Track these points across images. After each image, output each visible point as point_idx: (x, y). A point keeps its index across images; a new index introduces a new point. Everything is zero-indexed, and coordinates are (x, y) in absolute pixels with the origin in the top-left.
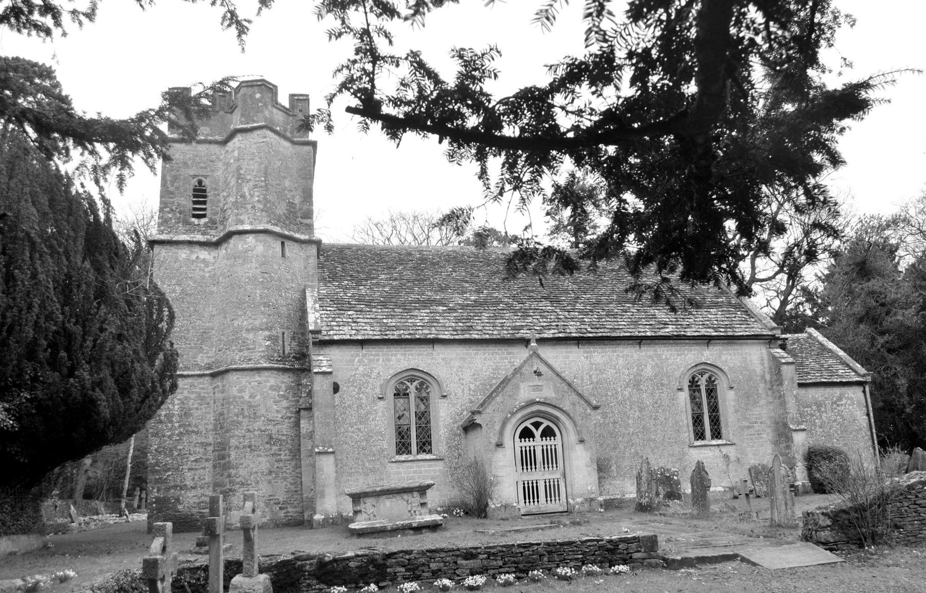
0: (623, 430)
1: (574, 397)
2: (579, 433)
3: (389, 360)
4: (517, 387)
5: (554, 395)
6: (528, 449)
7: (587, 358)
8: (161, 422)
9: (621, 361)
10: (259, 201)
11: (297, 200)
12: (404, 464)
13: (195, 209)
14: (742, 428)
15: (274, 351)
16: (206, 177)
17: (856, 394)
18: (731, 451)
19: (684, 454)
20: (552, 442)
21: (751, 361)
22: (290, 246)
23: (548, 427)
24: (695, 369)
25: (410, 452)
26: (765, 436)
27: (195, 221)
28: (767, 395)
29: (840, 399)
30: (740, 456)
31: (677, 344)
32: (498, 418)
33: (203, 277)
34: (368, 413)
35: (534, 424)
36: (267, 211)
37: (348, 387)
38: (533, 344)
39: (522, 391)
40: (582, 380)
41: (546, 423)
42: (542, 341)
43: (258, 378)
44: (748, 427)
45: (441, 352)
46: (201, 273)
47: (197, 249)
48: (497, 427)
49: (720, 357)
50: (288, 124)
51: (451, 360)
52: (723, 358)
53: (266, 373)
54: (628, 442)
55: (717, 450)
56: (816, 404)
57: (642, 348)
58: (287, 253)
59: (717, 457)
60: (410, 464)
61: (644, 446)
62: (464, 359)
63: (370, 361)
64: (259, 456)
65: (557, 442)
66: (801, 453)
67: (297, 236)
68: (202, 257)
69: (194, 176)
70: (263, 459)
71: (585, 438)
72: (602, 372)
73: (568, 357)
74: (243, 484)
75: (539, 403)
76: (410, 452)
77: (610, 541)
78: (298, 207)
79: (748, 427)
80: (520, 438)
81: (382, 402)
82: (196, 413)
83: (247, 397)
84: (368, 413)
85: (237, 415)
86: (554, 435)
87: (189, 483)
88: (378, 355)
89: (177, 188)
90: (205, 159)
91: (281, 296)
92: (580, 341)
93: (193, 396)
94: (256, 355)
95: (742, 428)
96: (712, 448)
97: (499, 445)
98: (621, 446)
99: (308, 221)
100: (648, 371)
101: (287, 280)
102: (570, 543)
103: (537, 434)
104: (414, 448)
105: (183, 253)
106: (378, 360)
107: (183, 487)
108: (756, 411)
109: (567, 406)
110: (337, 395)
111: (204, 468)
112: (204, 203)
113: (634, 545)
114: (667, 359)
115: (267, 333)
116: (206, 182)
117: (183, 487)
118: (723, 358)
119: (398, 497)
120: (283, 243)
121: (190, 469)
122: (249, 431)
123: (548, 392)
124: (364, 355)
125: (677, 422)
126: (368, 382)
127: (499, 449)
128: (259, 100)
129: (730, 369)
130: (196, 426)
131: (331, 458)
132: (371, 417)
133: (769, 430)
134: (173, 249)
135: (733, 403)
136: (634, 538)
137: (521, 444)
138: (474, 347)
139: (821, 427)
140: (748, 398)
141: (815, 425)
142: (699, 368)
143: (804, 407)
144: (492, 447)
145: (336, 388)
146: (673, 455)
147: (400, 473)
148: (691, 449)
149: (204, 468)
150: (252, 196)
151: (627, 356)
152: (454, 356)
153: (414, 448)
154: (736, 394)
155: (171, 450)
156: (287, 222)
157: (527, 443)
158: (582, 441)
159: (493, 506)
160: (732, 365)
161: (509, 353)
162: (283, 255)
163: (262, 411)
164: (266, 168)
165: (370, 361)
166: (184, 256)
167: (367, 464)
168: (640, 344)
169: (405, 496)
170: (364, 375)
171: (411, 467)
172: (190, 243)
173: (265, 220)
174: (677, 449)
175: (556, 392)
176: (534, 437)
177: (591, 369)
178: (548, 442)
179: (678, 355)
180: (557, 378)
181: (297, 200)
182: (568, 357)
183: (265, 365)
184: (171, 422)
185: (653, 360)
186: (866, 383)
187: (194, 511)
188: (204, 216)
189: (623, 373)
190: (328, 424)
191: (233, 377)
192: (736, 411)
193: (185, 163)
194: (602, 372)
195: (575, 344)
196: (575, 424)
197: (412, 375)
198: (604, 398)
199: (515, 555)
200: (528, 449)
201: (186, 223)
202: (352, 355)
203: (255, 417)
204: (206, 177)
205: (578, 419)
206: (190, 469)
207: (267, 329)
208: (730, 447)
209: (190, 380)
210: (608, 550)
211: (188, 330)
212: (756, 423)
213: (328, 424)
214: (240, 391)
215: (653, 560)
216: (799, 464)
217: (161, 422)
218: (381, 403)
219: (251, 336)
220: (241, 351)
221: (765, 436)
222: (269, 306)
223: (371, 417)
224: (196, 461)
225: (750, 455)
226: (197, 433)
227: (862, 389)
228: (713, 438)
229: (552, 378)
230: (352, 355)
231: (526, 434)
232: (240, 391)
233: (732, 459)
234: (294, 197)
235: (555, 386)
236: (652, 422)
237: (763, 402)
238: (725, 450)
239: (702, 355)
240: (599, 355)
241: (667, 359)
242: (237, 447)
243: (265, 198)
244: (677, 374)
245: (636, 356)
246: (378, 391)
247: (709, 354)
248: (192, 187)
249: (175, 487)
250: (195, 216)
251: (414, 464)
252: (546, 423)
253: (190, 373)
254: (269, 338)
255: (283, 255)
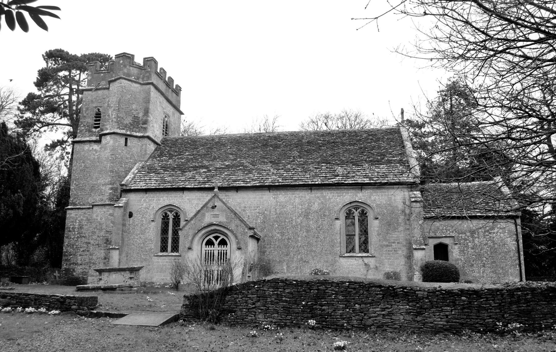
0: (293, 244)
1: (238, 222)
2: (238, 243)
3: (159, 200)
4: (204, 215)
5: (225, 220)
6: (225, 252)
7: (274, 198)
8: (70, 231)
9: (297, 200)
10: (115, 118)
11: (141, 115)
12: (162, 258)
13: (95, 124)
14: (382, 246)
15: (115, 195)
16: (101, 107)
17: (510, 226)
18: (372, 262)
19: (336, 261)
20: (225, 248)
21: (395, 200)
22: (130, 140)
23: (223, 239)
24: (349, 206)
25: (167, 251)
26: (400, 252)
27: (94, 130)
28: (406, 224)
29: (493, 228)
30: (378, 265)
31: (338, 189)
32: (191, 233)
33: (94, 158)
34: (146, 229)
35: (215, 237)
36: (118, 122)
37: (137, 214)
38: (216, 190)
39: (206, 218)
40: (270, 212)
41: (222, 237)
42: (220, 189)
43: (104, 210)
44: (387, 246)
45: (187, 195)
46: (94, 156)
47: (93, 144)
48: (190, 238)
49: (370, 197)
50: (141, 74)
51: (193, 199)
52: (373, 198)
53: (108, 207)
54: (296, 252)
55: (360, 260)
56: (470, 231)
57: (313, 192)
58: (129, 143)
59: (360, 265)
60: (164, 257)
61: (307, 254)
62: (200, 199)
63: (150, 200)
64: (101, 250)
65: (227, 248)
66: (419, 265)
67: (135, 134)
68: (94, 148)
69: (96, 107)
70: (103, 251)
71: (242, 247)
72: (284, 207)
73: (262, 198)
74: (94, 263)
75: (217, 225)
76: (167, 251)
77: (62, 297)
78: (140, 119)
79: (387, 246)
80: (206, 245)
81: (153, 223)
82: (85, 227)
83: (99, 219)
84: (146, 229)
85: (94, 228)
86: (227, 245)
87: (79, 262)
88: (154, 197)
89: (87, 114)
90: (101, 98)
91: (122, 166)
92: (270, 188)
93: (84, 219)
94: (105, 198)
95: (382, 246)
96: (357, 259)
97: (190, 248)
98: (292, 254)
99: (145, 126)
100: (316, 207)
101: (127, 158)
102: (45, 296)
103: (216, 243)
104: (169, 248)
105: (86, 147)
106: (154, 200)
107: (77, 264)
108: (395, 235)
109: (232, 227)
110: (131, 218)
111: (86, 255)
112: (99, 120)
113: (73, 301)
114: (330, 199)
115: (110, 186)
116: (101, 110)
117: (77, 264)
118: (373, 198)
119: (119, 273)
120: (126, 139)
121: (80, 255)
122: (98, 236)
123: (222, 219)
124: (147, 197)
125: (332, 240)
126: (147, 212)
127: (190, 251)
128: (122, 64)
129: (378, 205)
130: (85, 234)
131: (117, 252)
132: (147, 231)
133: (404, 248)
134: (82, 145)
135: (376, 229)
136: (74, 297)
137: (206, 249)
138: (206, 192)
139: (472, 248)
140: (390, 225)
141: (467, 246)
142: (352, 205)
143: (459, 234)
144: (186, 249)
145: (131, 215)
146: (327, 262)
147: (159, 262)
148: (341, 258)
149: (86, 255)
150: (112, 115)
151: (302, 197)
152: (194, 197)
153: (169, 248)
154: (380, 223)
155: (73, 245)
156: (132, 127)
157: (210, 248)
158: (239, 249)
159: (182, 283)
160: (379, 203)
161: (226, 196)
162: (126, 145)
163: (104, 227)
164: (120, 99)
165: (150, 200)
166: (87, 148)
167: (142, 256)
168: (311, 189)
169: (123, 273)
170: (146, 208)
171: (165, 259)
172: (90, 142)
173: (116, 127)
174: (330, 257)
175: (227, 218)
176: (214, 245)
177: (277, 205)
178: (223, 248)
179: (338, 196)
180: (228, 210)
181: (141, 115)
182: (262, 198)
183: (108, 203)
184: (74, 231)
185: (320, 200)
186: (517, 217)
187: (81, 276)
188: (99, 127)
189: (298, 208)
190: (118, 234)
191: (95, 209)
192: (379, 235)
193: (92, 101)
194: (284, 207)
195: (267, 190)
196: (236, 237)
197: (170, 208)
198: (283, 224)
199: (21, 299)
200: (225, 252)
201: (90, 131)
202: (141, 198)
203: (101, 229)
204: (101, 107)
205: (239, 235)
206: (80, 255)
207: (111, 184)
208: (370, 259)
209: (84, 211)
210: (61, 302)
211: (86, 186)
212: (394, 243)
213: (118, 234)
214: (97, 216)
215: (81, 311)
216: (417, 273)
217: (70, 231)
218: (153, 223)
219: (104, 188)
220: (99, 195)
221: (400, 252)
222: (113, 172)
223: (147, 231)
224: (83, 251)
225: (387, 265)
226: (85, 237)
227: (513, 221)
228: (172, 251)
229: (225, 210)
230: (141, 198)
231: (210, 243)
232: (97, 216)
233: (372, 266)
234: (138, 113)
235: (227, 215)
236: (315, 239)
237: (401, 228)
238: (366, 260)
239: (356, 196)
240: (283, 197)
241: (330, 199)
242: (93, 245)
243: (118, 116)
244: (337, 208)
245: (308, 197)
246: (152, 217)
247: (361, 196)
248: (94, 113)
249: (73, 263)
250: (96, 128)
251: (167, 258)
252: (222, 237)
253: (84, 207)
254: (112, 189)
255: (126, 145)
